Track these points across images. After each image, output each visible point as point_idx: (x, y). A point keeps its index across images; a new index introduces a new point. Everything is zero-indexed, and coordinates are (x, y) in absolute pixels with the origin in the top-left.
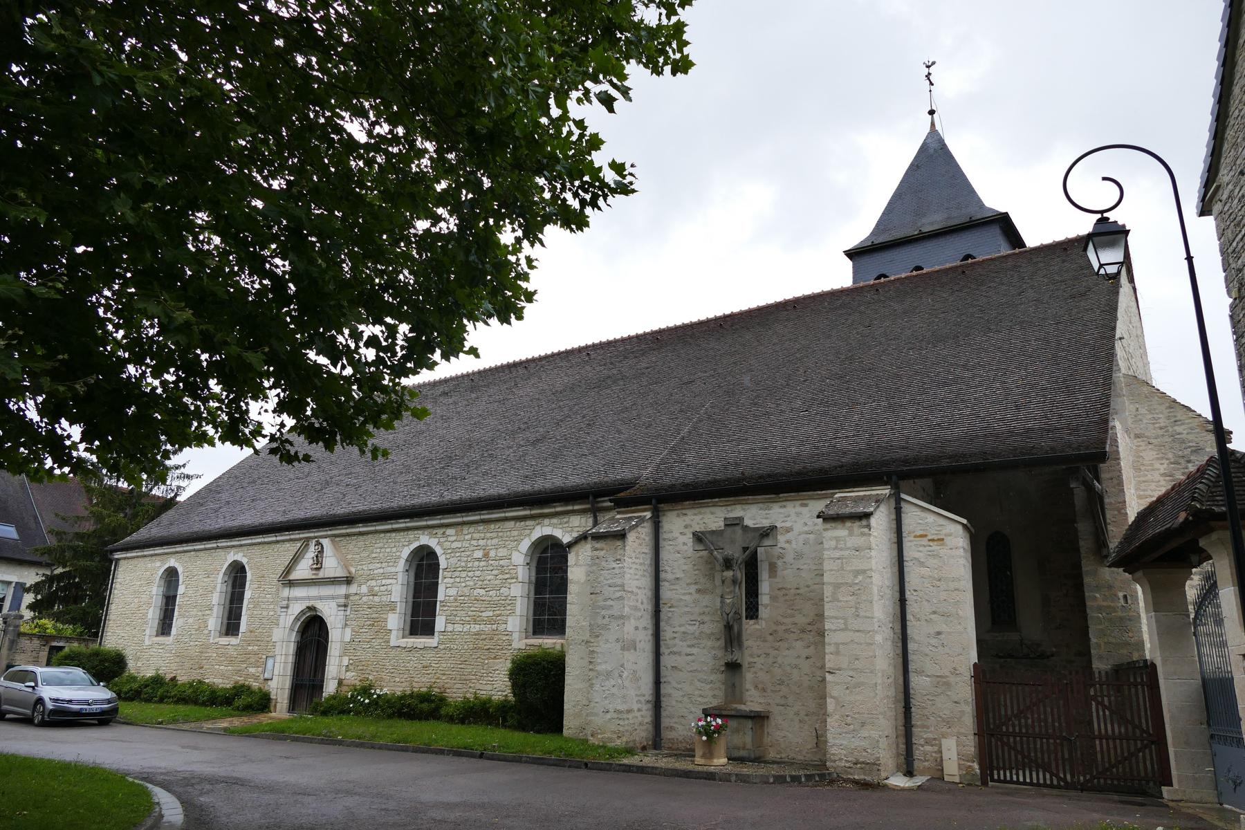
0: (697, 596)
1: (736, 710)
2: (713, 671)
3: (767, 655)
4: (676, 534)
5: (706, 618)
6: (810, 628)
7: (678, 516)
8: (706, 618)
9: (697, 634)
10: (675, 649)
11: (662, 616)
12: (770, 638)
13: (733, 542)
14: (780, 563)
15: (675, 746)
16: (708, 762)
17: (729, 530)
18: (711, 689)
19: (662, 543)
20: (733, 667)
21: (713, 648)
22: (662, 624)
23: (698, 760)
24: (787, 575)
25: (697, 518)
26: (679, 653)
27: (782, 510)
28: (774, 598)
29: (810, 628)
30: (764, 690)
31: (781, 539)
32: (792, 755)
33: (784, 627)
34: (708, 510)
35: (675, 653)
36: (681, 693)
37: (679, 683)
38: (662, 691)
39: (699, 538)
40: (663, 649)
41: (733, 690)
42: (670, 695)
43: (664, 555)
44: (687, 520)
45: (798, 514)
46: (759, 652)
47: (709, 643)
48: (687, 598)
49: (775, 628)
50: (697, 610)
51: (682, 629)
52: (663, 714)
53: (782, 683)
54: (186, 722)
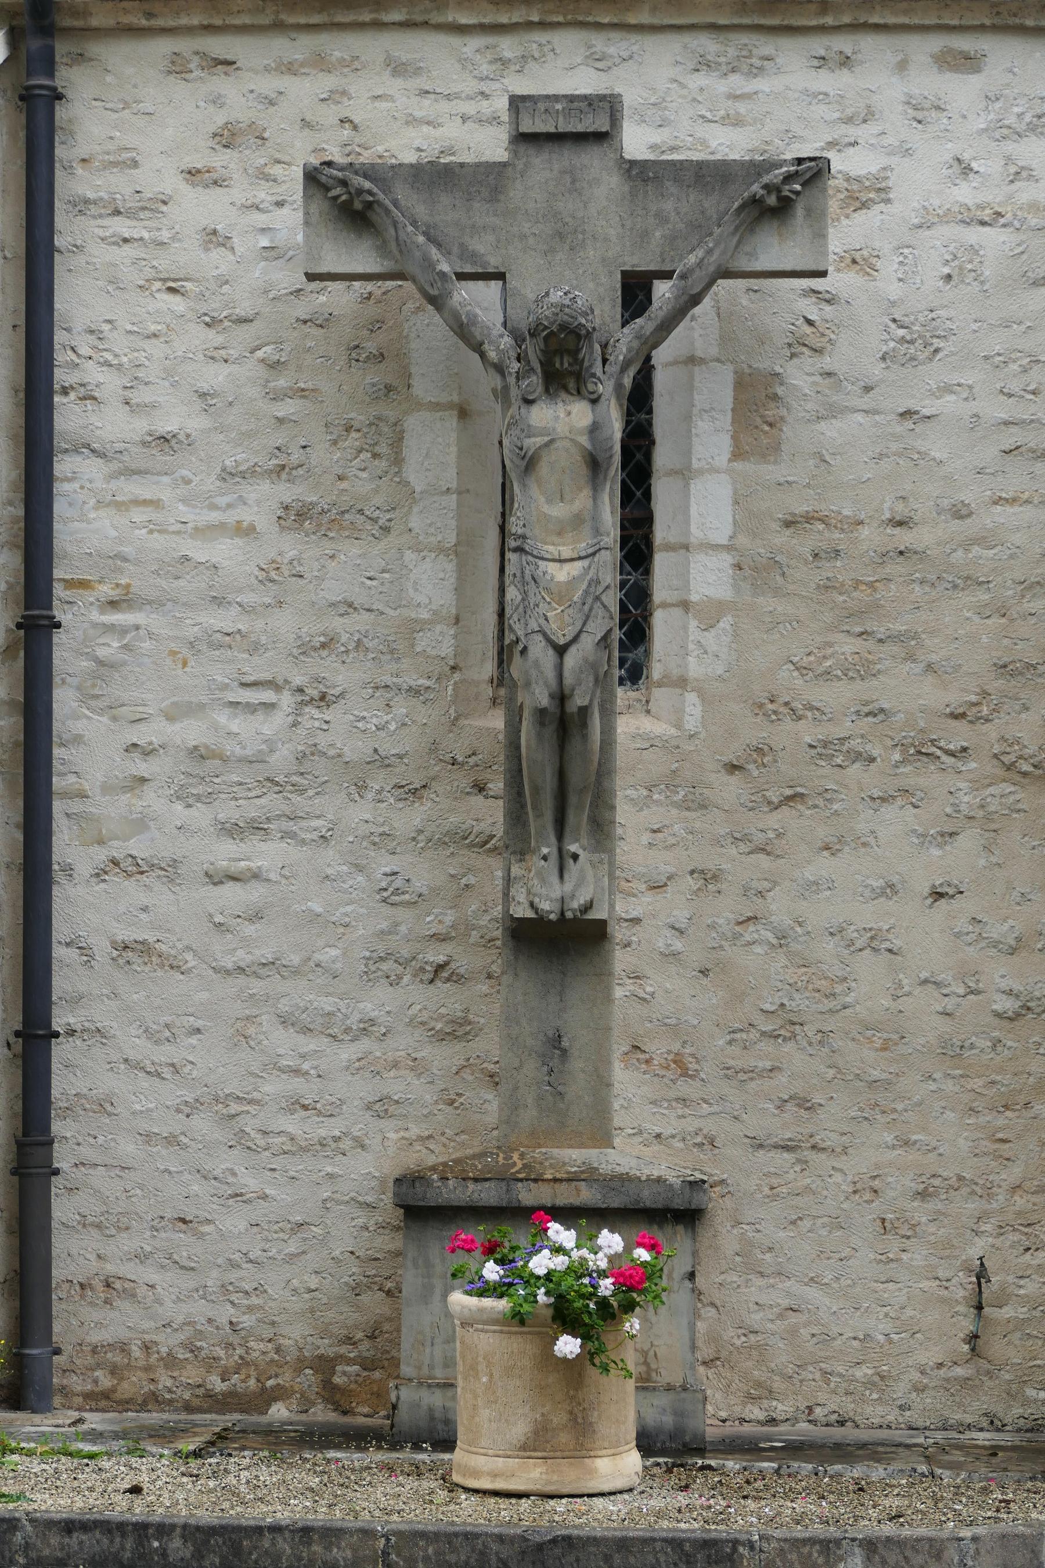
0: (290, 546)
1: (589, 1175)
2: (382, 965)
3: (708, 878)
4: (160, 176)
5: (341, 676)
6: (959, 735)
7: (177, 68)
8: (341, 676)
9: (282, 758)
10: (138, 847)
11: (66, 654)
12: (730, 790)
13: (565, 236)
14: (800, 377)
15: (133, 1385)
16: (568, 1477)
17: (544, 167)
18: (360, 1066)
19: (67, 229)
20: (561, 944)
21: (383, 839)
22: (64, 700)
23: (488, 1456)
24: (840, 446)
25: (304, 91)
26: (169, 870)
27: (827, 81)
28: (756, 572)
29: (959, 735)
30: (681, 1066)
31: (845, 233)
32: (829, 1404)
33: (808, 732)
34: (371, 47)
35: (136, 868)
36: (174, 1093)
37: (168, 1035)
38: (62, 1085)
39: (349, 201)
40: (66, 844)
41: (557, 1070)
42: (104, 1106)
43: (77, 300)
44: (237, 97)
45: (921, 111)
46: (663, 863)
47: (361, 813)
48: (224, 552)
49: (753, 731)
50: (286, 625)
51: (192, 732)
52: (62, 1209)
53: (787, 1026)
54: (535, 1450)
